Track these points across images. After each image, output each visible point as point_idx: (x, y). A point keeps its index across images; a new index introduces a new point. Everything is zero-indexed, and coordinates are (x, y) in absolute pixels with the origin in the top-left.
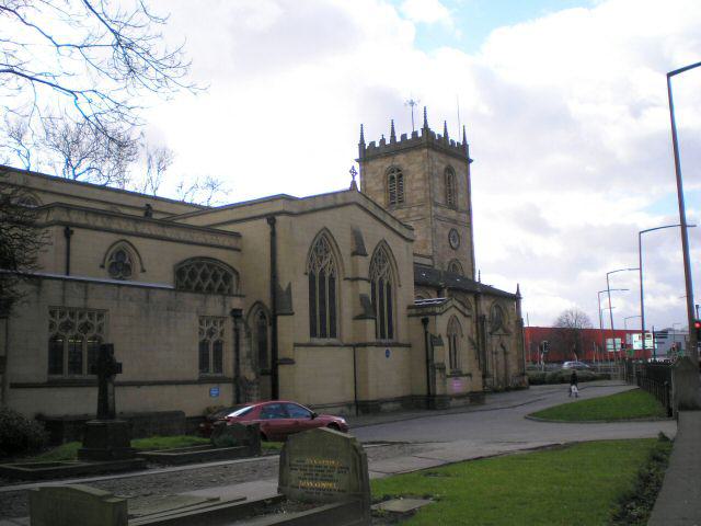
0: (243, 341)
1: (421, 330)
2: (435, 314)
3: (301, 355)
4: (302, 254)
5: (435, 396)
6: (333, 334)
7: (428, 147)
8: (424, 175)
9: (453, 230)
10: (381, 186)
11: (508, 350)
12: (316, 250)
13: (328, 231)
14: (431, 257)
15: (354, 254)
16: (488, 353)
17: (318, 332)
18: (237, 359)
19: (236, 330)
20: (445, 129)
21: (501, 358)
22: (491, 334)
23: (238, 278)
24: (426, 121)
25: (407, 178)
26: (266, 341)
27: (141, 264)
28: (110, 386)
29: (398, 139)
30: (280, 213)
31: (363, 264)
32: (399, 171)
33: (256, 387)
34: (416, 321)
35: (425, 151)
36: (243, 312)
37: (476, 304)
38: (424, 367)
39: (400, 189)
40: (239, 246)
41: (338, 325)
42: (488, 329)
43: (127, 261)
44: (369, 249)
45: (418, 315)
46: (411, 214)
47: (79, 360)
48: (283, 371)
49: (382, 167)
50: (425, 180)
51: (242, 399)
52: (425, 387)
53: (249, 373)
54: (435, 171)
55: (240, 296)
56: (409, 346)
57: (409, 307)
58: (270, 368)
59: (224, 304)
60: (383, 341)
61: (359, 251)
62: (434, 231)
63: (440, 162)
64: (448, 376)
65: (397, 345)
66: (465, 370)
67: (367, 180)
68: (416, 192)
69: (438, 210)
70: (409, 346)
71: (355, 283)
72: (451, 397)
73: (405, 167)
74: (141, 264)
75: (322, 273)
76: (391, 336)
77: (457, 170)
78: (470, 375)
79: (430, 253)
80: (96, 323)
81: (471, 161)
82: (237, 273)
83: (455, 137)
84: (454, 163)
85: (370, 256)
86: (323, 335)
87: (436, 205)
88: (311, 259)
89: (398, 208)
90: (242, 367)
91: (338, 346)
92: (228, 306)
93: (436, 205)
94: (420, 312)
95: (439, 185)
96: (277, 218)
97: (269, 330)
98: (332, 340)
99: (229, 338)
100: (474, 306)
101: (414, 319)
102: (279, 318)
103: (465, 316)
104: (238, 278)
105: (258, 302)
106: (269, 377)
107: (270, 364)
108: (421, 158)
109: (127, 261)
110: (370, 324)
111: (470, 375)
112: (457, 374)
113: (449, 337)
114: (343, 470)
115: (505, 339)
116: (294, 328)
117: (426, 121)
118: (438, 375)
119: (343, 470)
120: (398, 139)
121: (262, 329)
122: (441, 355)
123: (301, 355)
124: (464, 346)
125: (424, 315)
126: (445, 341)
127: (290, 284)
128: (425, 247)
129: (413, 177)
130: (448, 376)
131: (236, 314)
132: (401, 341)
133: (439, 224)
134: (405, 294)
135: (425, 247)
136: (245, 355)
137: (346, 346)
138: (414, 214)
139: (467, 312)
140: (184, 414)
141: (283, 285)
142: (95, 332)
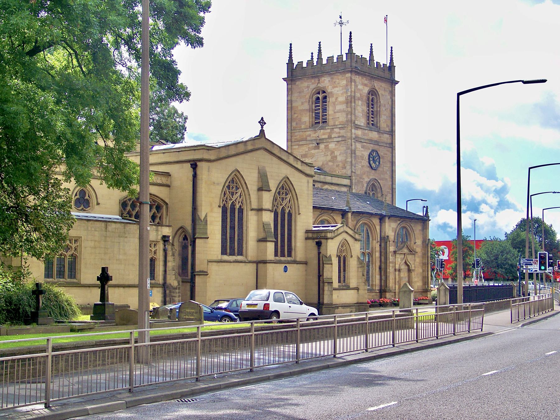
0: (169, 258)
1: (315, 252)
2: (327, 239)
3: (214, 269)
4: (218, 191)
5: (323, 304)
6: (240, 253)
7: (351, 72)
8: (347, 99)
9: (373, 151)
10: (306, 106)
11: (412, 267)
12: (228, 187)
13: (239, 172)
14: (350, 178)
15: (260, 189)
16: (391, 270)
17: (228, 251)
18: (165, 271)
19: (165, 251)
20: (371, 52)
21: (404, 274)
22: (395, 252)
23: (167, 208)
24: (350, 46)
25: (330, 100)
26: (187, 257)
27: (97, 199)
28: (106, 287)
29: (324, 62)
30: (201, 160)
31: (267, 200)
32: (324, 92)
33: (177, 291)
34: (312, 244)
35: (348, 75)
36: (171, 238)
37: (381, 226)
38: (316, 280)
39: (325, 110)
40: (168, 183)
41: (244, 246)
42: (392, 249)
43: (87, 197)
44: (273, 185)
45: (313, 239)
46: (333, 136)
47: (62, 269)
48: (198, 279)
49: (308, 87)
50: (347, 103)
51: (168, 299)
52: (317, 300)
53: (173, 281)
54: (358, 95)
55: (169, 226)
56: (306, 263)
57: (307, 232)
58: (189, 277)
59: (157, 230)
60: (282, 259)
61: (263, 188)
62: (353, 152)
63: (362, 86)
64: (335, 289)
65: (295, 262)
66: (353, 284)
67: (293, 99)
68: (338, 115)
69: (359, 132)
70: (306, 263)
71: (260, 212)
72: (337, 307)
73: (329, 90)
74: (97, 199)
75: (233, 205)
76: (290, 255)
77: (380, 92)
78: (357, 289)
79: (349, 173)
80: (74, 246)
81: (397, 82)
82: (167, 204)
83: (381, 58)
84: (381, 87)
85: (273, 189)
86: (232, 254)
87: (357, 127)
88: (225, 194)
89: (322, 128)
90: (168, 277)
91: (245, 262)
92: (160, 233)
93: (357, 127)
94: (315, 236)
95: (361, 108)
96: (198, 163)
97: (190, 248)
98: (239, 258)
99: (160, 256)
100: (378, 228)
101: (310, 241)
102: (197, 241)
103: (356, 240)
104: (167, 208)
105: (181, 228)
106: (189, 284)
107: (189, 273)
108: (344, 82)
109: (87, 197)
110: (270, 247)
111: (357, 289)
112: (345, 286)
113: (339, 257)
114: (196, 313)
115: (410, 258)
116: (210, 246)
117: (350, 46)
118: (326, 288)
119: (196, 313)
120: (324, 62)
121: (185, 247)
122: (332, 272)
123: (214, 269)
124: (353, 264)
125: (318, 239)
126: (335, 261)
127: (206, 216)
128: (344, 168)
129: (336, 99)
130: (335, 289)
131: (165, 239)
132: (298, 259)
133: (359, 145)
134: (305, 220)
135: (344, 168)
136: (171, 268)
137: (250, 262)
138: (336, 135)
139: (357, 236)
140: (129, 307)
141: (202, 214)
142: (73, 251)
